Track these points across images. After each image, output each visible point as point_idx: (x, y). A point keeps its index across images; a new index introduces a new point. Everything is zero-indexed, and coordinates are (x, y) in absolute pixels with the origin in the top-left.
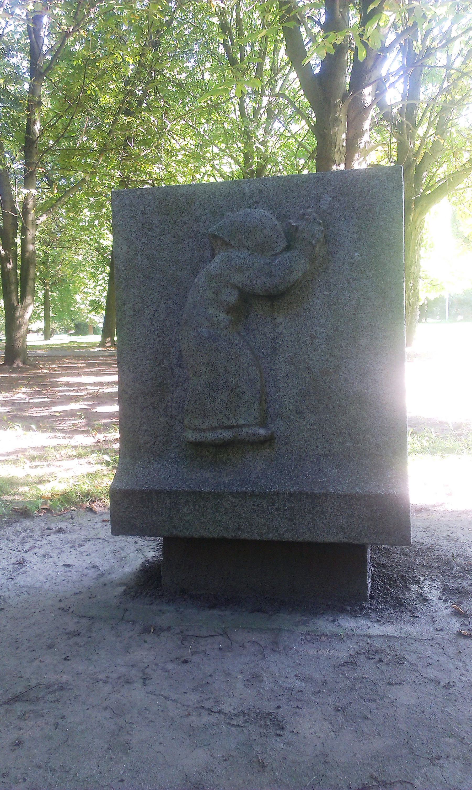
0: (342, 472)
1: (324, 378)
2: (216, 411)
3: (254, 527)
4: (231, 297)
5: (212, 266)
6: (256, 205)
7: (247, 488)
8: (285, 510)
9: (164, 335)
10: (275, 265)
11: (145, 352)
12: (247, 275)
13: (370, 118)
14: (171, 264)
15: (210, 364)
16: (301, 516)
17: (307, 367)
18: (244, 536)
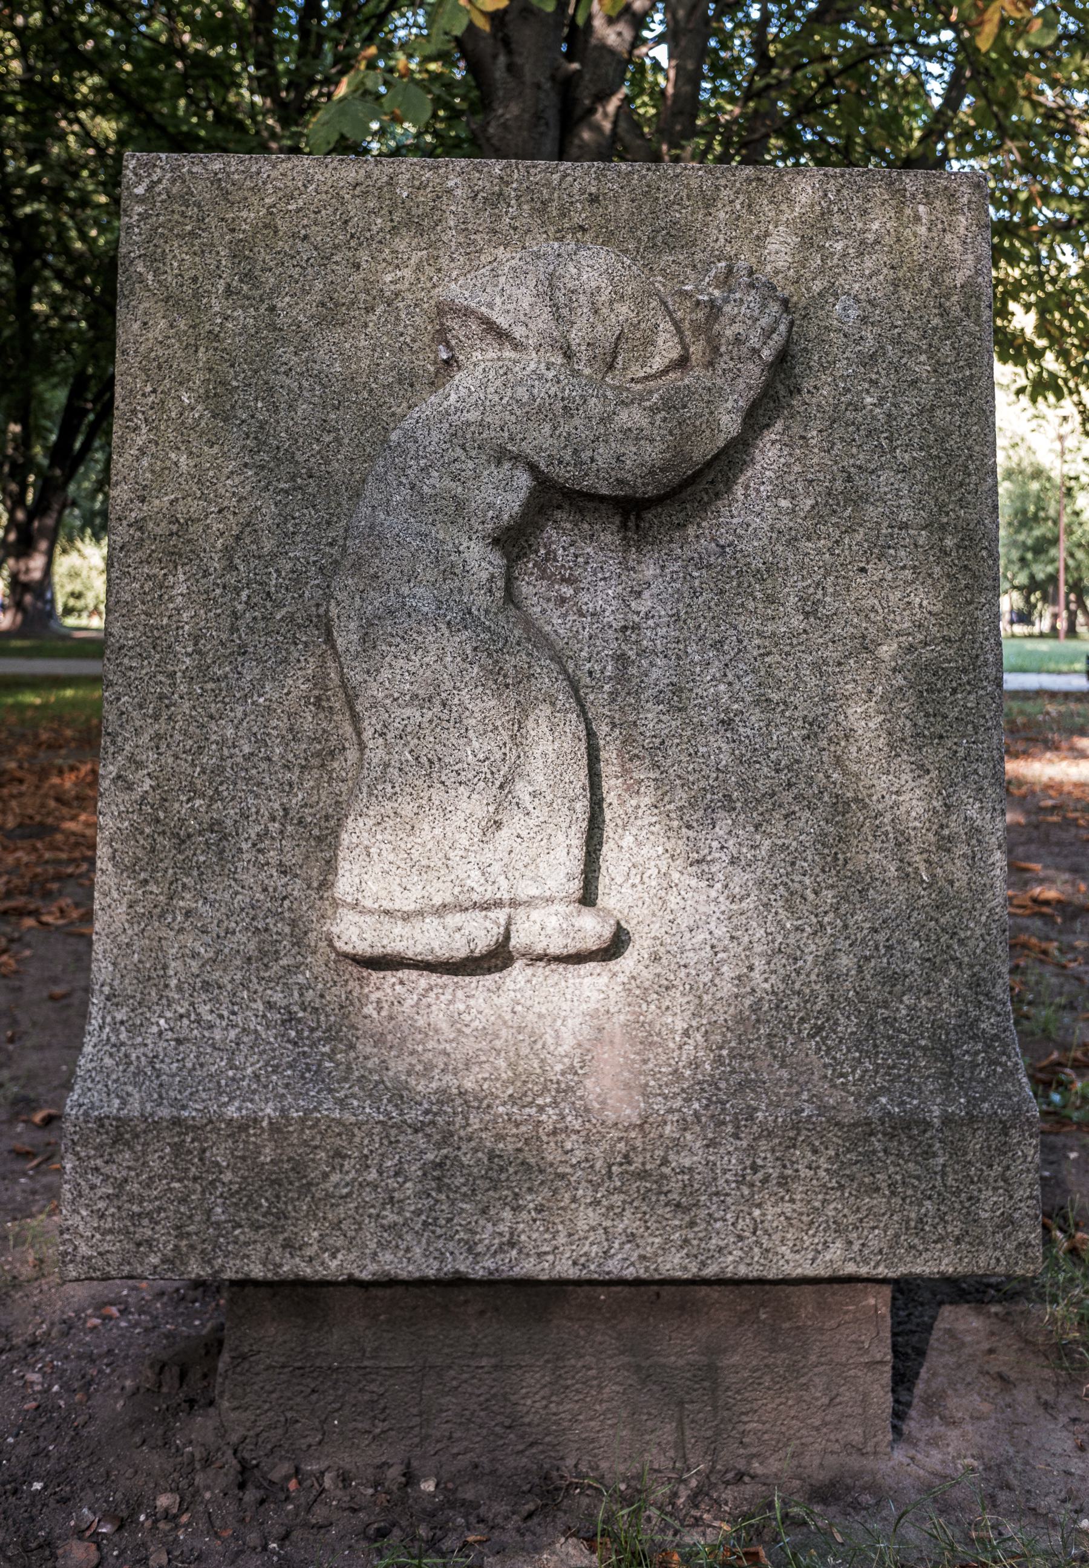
0: (829, 1049)
1: (773, 756)
2: (451, 854)
3: (562, 1239)
4: (506, 495)
5: (453, 397)
6: (579, 235)
7: (541, 1109)
8: (663, 1176)
9: (269, 604)
10: (651, 409)
11: (199, 652)
12: (564, 429)
13: (620, 95)
14: (305, 384)
15: (437, 701)
16: (717, 1194)
17: (723, 722)
18: (528, 1267)
